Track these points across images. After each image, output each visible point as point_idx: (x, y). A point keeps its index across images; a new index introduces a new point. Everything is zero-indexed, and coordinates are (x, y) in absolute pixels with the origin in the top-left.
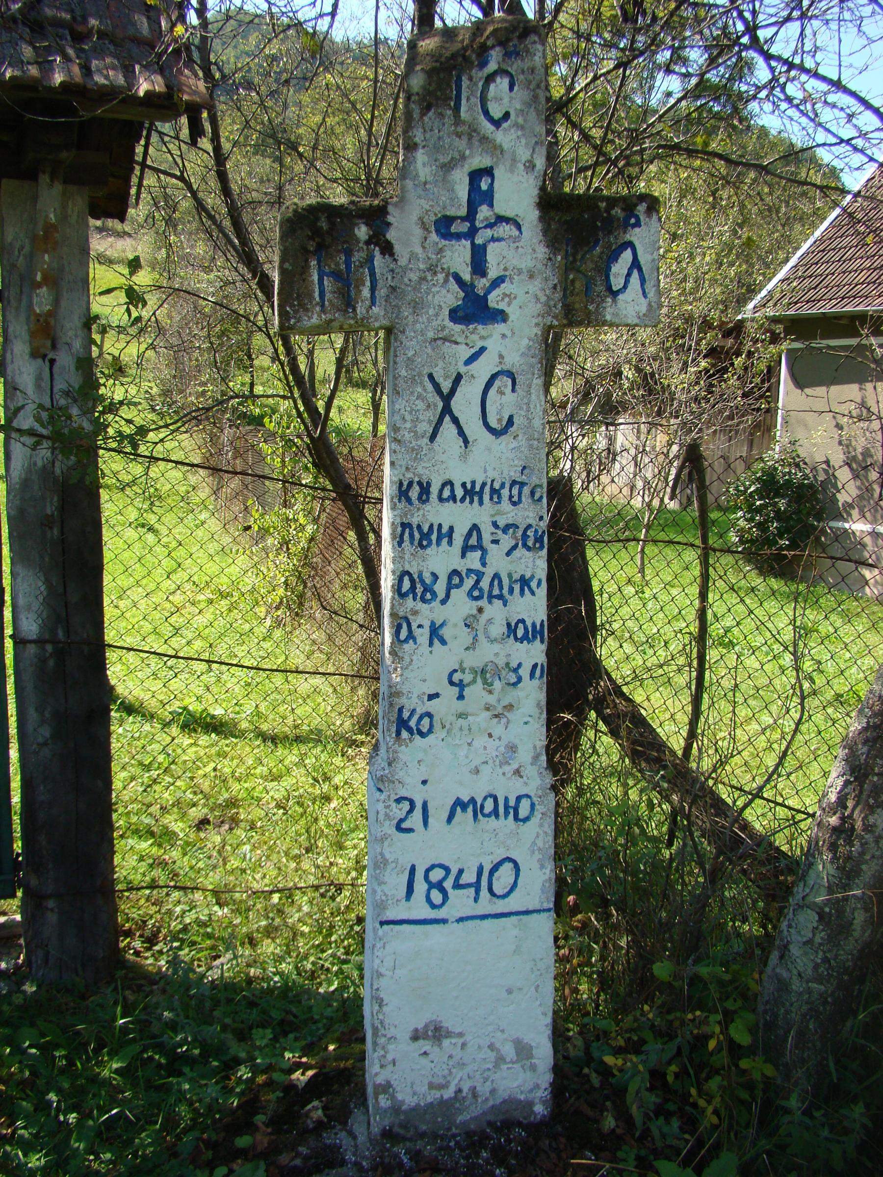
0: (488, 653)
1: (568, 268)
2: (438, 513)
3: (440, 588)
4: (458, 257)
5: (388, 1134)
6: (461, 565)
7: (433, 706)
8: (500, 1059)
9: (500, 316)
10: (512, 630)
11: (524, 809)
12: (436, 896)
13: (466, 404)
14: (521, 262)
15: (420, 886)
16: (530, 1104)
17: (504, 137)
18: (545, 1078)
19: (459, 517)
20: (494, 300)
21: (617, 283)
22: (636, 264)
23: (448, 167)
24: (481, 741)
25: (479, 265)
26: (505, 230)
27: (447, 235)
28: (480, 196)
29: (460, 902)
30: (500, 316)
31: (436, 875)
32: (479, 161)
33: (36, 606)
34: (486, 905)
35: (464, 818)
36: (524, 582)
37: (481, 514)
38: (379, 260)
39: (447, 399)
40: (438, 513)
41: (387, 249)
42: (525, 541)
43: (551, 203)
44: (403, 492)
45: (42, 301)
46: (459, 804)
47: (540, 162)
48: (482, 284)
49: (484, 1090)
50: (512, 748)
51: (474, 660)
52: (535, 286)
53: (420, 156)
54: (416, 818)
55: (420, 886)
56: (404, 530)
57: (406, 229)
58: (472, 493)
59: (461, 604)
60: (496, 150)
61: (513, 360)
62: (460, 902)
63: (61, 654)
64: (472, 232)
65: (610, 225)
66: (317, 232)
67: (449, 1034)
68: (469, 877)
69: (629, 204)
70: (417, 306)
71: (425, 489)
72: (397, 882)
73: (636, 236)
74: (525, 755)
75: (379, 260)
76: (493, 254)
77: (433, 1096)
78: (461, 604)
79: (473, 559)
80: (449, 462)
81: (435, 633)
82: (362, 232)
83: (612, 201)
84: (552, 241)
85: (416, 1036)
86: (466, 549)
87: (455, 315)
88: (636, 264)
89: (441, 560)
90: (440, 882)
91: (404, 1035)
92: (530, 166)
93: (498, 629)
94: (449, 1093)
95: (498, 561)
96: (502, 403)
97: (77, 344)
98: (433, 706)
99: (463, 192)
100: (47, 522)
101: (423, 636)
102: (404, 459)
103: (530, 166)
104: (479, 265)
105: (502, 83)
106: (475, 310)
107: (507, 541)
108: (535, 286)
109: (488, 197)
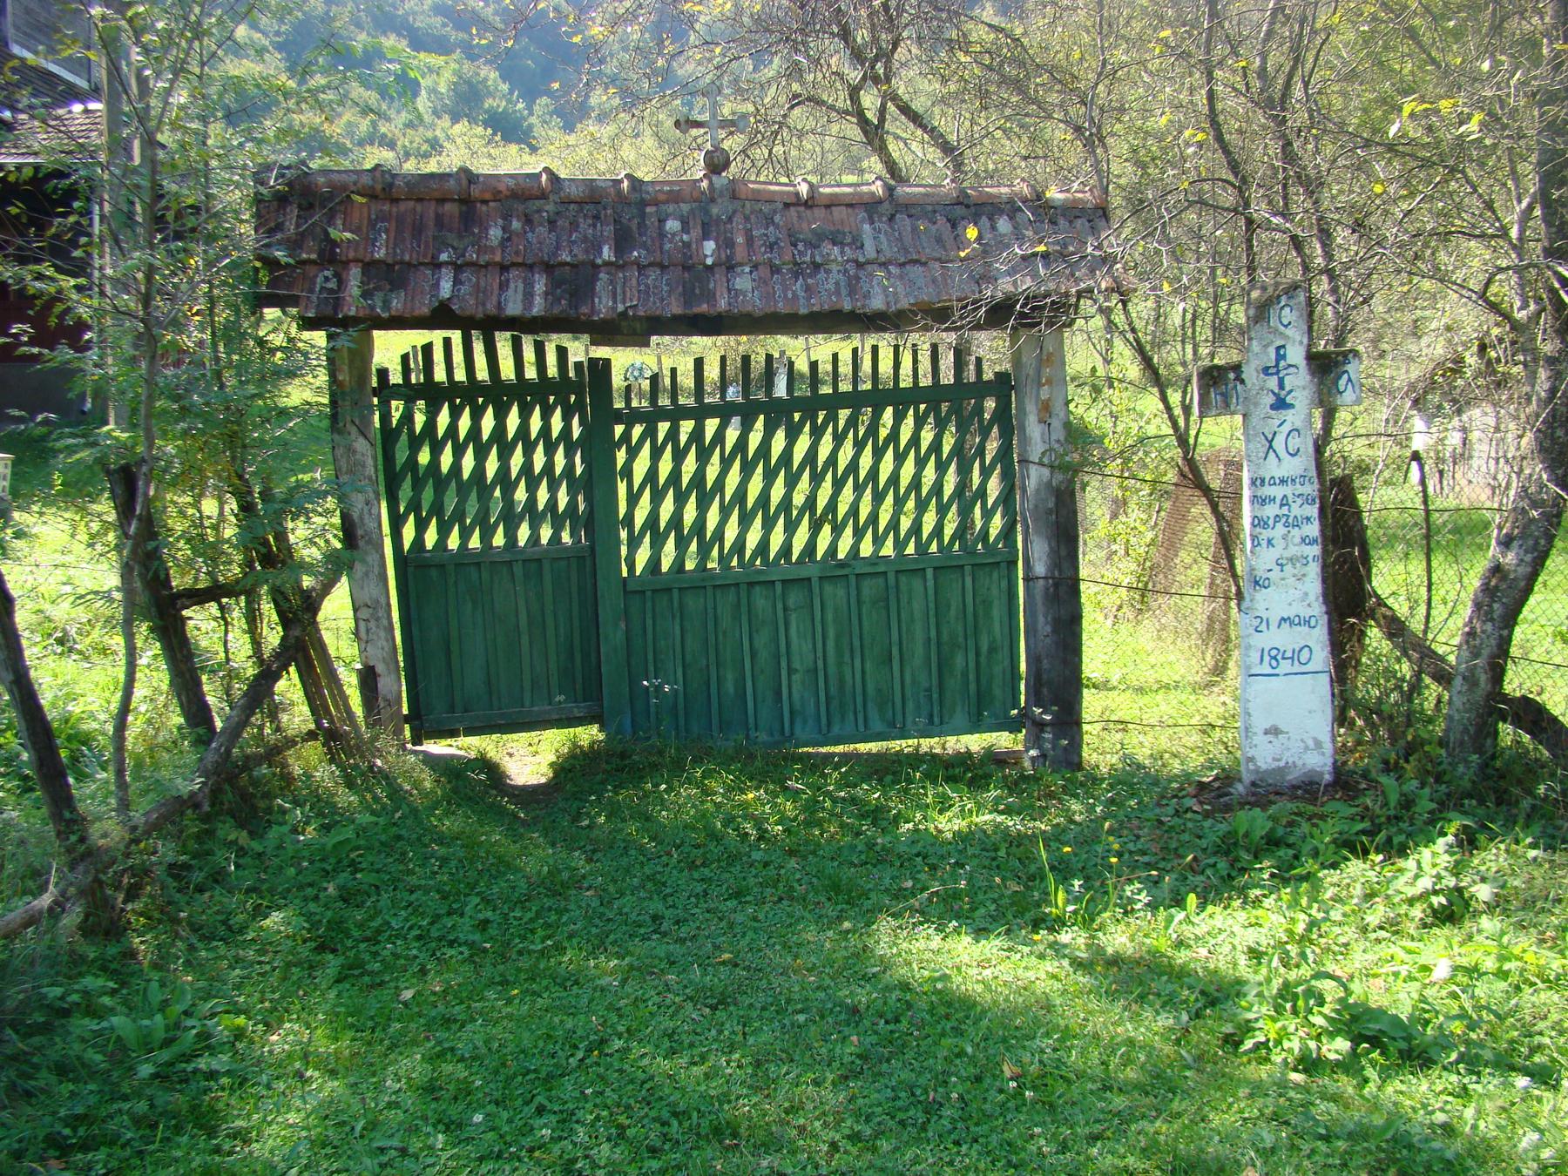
0: (1294, 550)
1: (1321, 383)
2: (1268, 491)
3: (1271, 522)
4: (1272, 383)
5: (1253, 784)
6: (1280, 513)
7: (1269, 575)
8: (1307, 748)
9: (1291, 406)
10: (1303, 540)
11: (1313, 623)
12: (1274, 663)
13: (1278, 444)
14: (1299, 382)
15: (1266, 658)
16: (1322, 774)
17: (1289, 332)
18: (1329, 761)
19: (1278, 492)
20: (1288, 400)
21: (1341, 388)
22: (1349, 380)
23: (1266, 346)
24: (1292, 591)
25: (1281, 386)
26: (1292, 370)
27: (1267, 375)
28: (1280, 357)
29: (1285, 666)
30: (1291, 406)
31: (1274, 652)
32: (1279, 343)
33: (1045, 558)
34: (1297, 668)
35: (1285, 626)
36: (1308, 519)
37: (1287, 490)
38: (1239, 387)
39: (1270, 442)
40: (1268, 491)
41: (1242, 382)
42: (1308, 501)
43: (1311, 357)
44: (1253, 483)
45: (1045, 393)
46: (1283, 619)
47: (1305, 341)
48: (1283, 393)
49: (1299, 763)
50: (1306, 594)
51: (1287, 554)
52: (1306, 393)
53: (1254, 343)
54: (1263, 627)
55: (1266, 658)
56: (1254, 498)
57: (1249, 373)
58: (1283, 481)
59: (1280, 529)
60: (1287, 337)
61: (1298, 424)
62: (1285, 666)
63: (1056, 585)
64: (1278, 373)
65: (1337, 364)
66: (1213, 377)
67: (1282, 732)
68: (1289, 654)
69: (1345, 355)
70: (1256, 404)
71: (1263, 481)
72: (1255, 656)
73: (1348, 367)
74: (1312, 597)
75: (1239, 387)
76: (1287, 381)
77: (1275, 765)
78: (1280, 529)
79: (1285, 510)
80: (1272, 469)
81: (1269, 542)
82: (1232, 376)
83: (1338, 354)
84: (1313, 373)
85: (1266, 733)
86: (1282, 505)
87: (1273, 407)
88: (1349, 380)
89: (1270, 511)
90: (1276, 656)
91: (1260, 731)
92: (1301, 343)
93: (1297, 540)
94: (1282, 764)
95: (1296, 510)
96: (1294, 443)
97: (1062, 414)
98: (1269, 575)
99: (1273, 356)
100: (1049, 512)
101: (1264, 544)
102: (1253, 468)
103: (1301, 343)
104: (1281, 386)
105: (1287, 310)
106: (1281, 404)
107: (1299, 501)
108: (1306, 393)
109: (1284, 357)
